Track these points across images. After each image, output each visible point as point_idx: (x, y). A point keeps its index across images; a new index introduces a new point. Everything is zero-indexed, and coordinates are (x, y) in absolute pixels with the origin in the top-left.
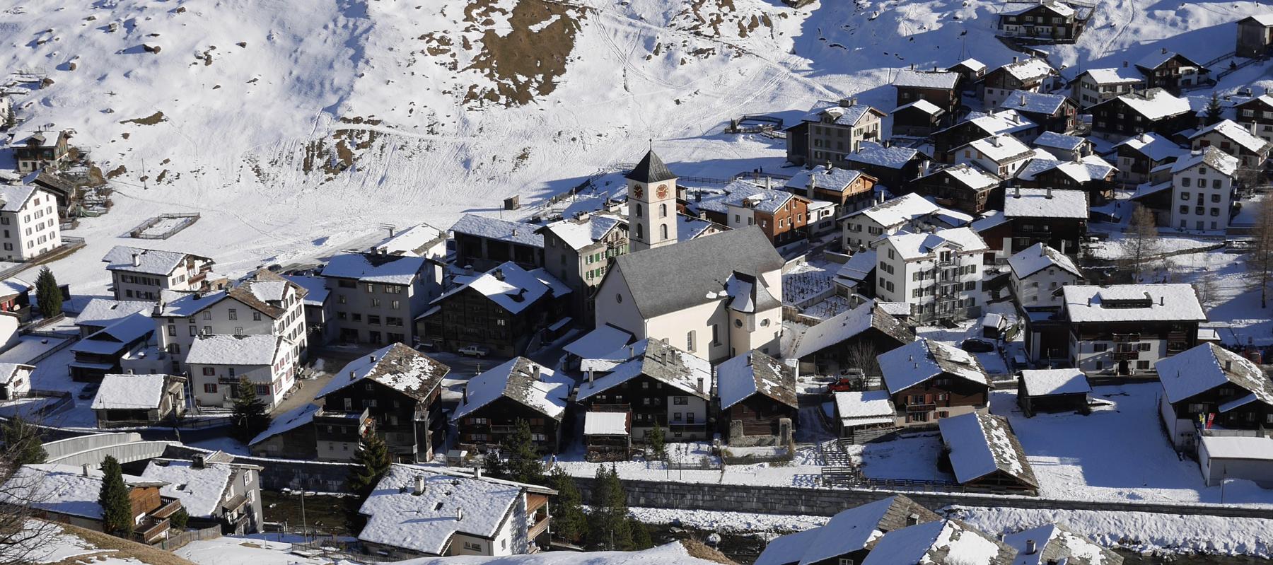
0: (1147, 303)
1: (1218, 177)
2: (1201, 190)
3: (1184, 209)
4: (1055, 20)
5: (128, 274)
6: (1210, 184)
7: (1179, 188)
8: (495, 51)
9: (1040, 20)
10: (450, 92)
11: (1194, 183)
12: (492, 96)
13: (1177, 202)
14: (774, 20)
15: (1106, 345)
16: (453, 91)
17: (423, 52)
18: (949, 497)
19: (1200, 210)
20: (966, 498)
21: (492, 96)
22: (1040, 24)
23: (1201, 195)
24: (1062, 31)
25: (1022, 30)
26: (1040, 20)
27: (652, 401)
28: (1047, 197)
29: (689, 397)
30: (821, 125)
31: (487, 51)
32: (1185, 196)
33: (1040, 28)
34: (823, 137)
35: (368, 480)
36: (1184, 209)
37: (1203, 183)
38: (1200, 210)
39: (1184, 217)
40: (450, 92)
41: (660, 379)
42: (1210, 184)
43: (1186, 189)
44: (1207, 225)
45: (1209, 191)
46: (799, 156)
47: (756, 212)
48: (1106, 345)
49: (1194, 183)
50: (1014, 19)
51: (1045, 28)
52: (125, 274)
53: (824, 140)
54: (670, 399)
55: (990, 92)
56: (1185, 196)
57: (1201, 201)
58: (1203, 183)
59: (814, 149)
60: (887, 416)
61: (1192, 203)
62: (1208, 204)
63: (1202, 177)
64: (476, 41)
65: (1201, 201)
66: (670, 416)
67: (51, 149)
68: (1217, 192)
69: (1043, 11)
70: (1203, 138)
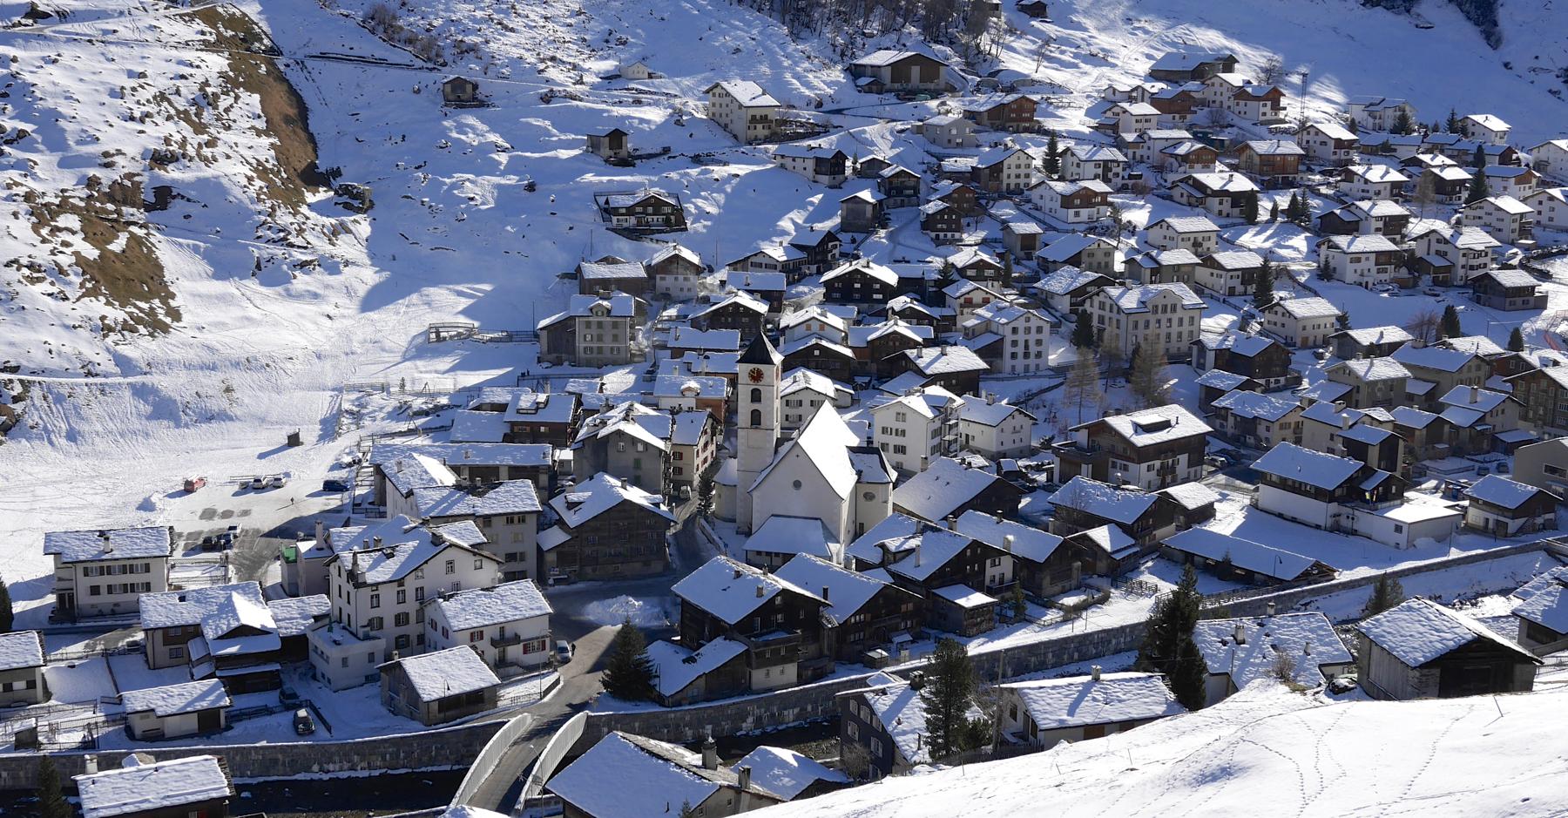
0: (1165, 425)
2: (1027, 337)
5: (139, 562)
6: (1034, 330)
7: (1009, 338)
8: (98, 277)
9: (650, 210)
10: (80, 326)
11: (1021, 331)
12: (126, 327)
13: (1008, 349)
14: (351, 226)
16: (83, 324)
17: (19, 281)
18: (1303, 591)
19: (1026, 355)
20: (1313, 589)
21: (126, 327)
22: (650, 215)
23: (1026, 341)
26: (650, 210)
30: (591, 319)
31: (88, 276)
32: (1015, 343)
33: (650, 218)
34: (594, 331)
35: (64, 760)
37: (1028, 330)
38: (1026, 355)
39: (1014, 362)
40: (80, 326)
42: (1034, 330)
43: (1015, 337)
44: (1032, 368)
45: (1033, 337)
46: (555, 355)
50: (624, 211)
51: (655, 218)
52: (88, 565)
53: (595, 334)
55: (662, 279)
57: (1027, 347)
58: (1028, 330)
59: (583, 345)
60: (1129, 547)
61: (1020, 350)
62: (1033, 349)
63: (1028, 325)
64: (69, 266)
65: (1027, 347)
68: (1039, 337)
70: (967, 296)
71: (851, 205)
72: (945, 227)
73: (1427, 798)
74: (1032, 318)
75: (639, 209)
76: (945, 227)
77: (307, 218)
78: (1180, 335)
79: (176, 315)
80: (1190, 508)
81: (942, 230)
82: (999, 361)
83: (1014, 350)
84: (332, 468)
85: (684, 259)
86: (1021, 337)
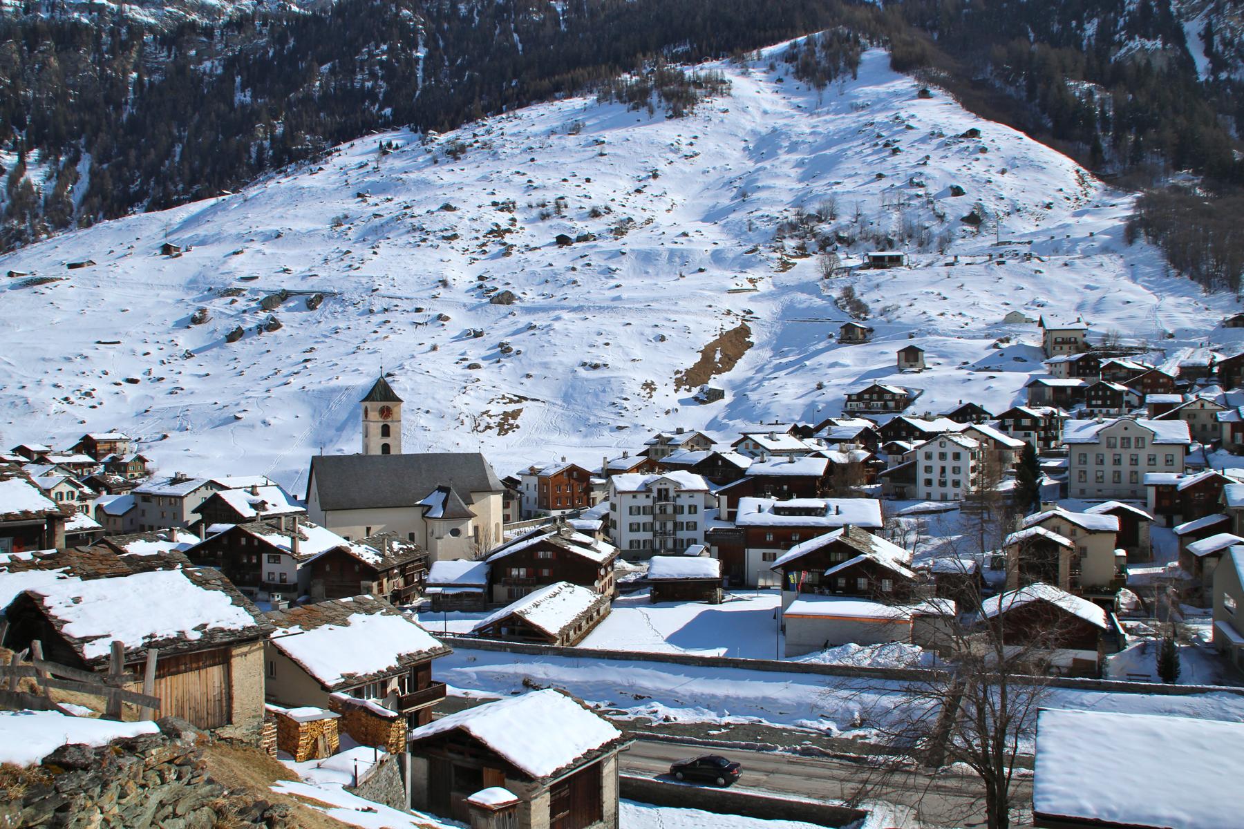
1: (958, 449)
3: (929, 482)
4: (887, 397)
6: (950, 456)
9: (875, 397)
11: (936, 456)
13: (922, 476)
15: (775, 554)
24: (892, 404)
25: (862, 405)
26: (875, 397)
27: (250, 560)
28: (790, 462)
29: (282, 556)
32: (928, 469)
36: (929, 482)
41: (258, 535)
42: (950, 456)
43: (928, 463)
45: (949, 463)
47: (540, 478)
48: (775, 554)
49: (936, 456)
51: (879, 403)
54: (265, 556)
56: (928, 469)
58: (943, 456)
61: (935, 476)
62: (950, 476)
63: (942, 450)
66: (265, 577)
67: (126, 465)
69: (877, 389)
71: (1035, 389)
72: (1099, 402)
73: (533, 400)
74: (948, 443)
75: (866, 396)
76: (1099, 402)
77: (477, 231)
78: (1117, 474)
79: (631, 542)
80: (742, 499)
81: (1096, 406)
82: (912, 487)
83: (928, 476)
84: (520, 411)
85: (1066, 536)
86: (936, 463)
